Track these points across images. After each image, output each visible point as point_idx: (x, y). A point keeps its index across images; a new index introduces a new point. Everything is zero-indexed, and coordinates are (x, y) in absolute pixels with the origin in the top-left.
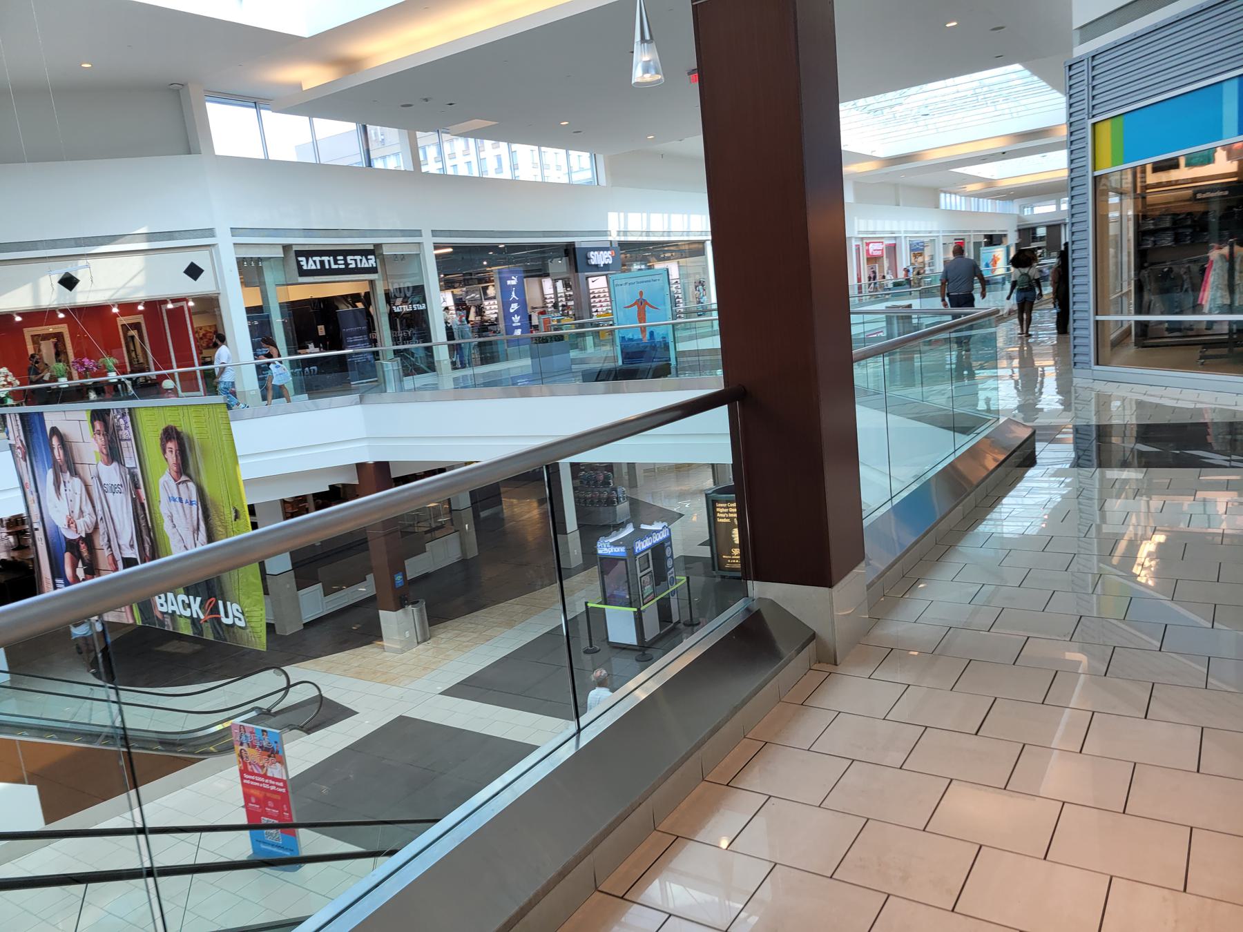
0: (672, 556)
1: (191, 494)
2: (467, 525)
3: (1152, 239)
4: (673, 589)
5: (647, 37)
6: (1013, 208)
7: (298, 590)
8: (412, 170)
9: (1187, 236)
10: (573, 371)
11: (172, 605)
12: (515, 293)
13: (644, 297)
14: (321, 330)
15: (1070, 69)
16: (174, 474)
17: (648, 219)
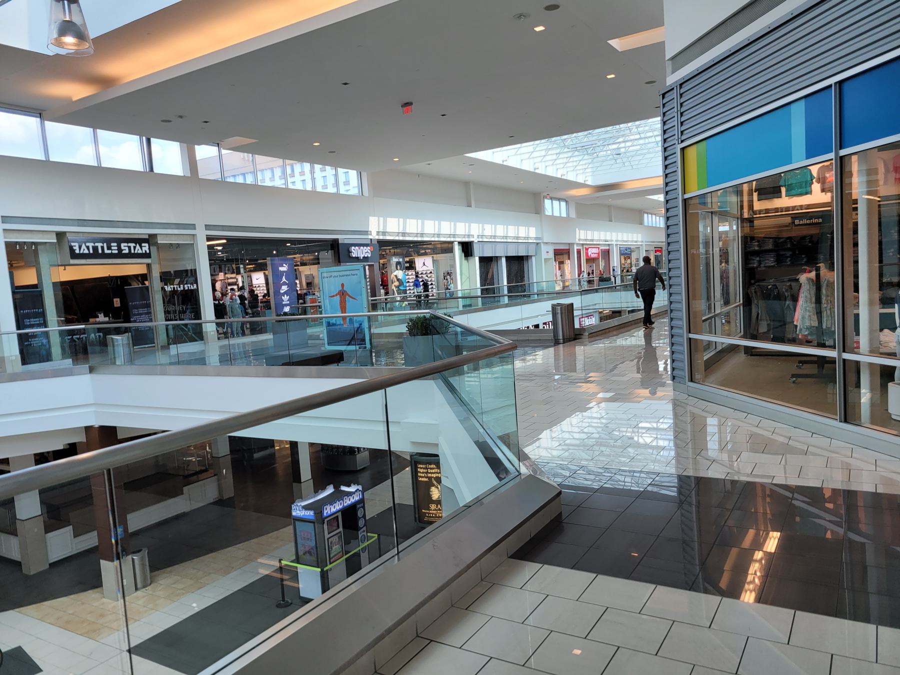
0: (364, 516)
2: (224, 471)
3: (758, 259)
4: (364, 546)
7: (46, 532)
8: (190, 176)
9: (787, 257)
10: (309, 345)
12: (285, 277)
14: (117, 302)
15: (663, 98)
17: (423, 224)
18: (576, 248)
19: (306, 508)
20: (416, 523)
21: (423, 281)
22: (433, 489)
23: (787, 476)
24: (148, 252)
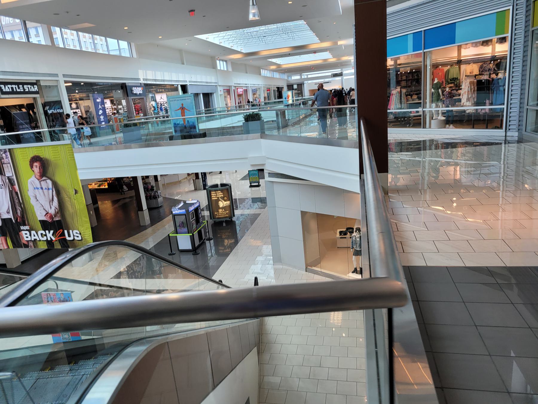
1: (49, 185)
5: (255, 3)
6: (285, 77)
11: (34, 236)
13: (184, 106)
16: (38, 177)
18: (233, 88)
19: (180, 209)
20: (211, 220)
21: (164, 108)
22: (220, 202)
23: (145, 331)
24: (37, 90)
